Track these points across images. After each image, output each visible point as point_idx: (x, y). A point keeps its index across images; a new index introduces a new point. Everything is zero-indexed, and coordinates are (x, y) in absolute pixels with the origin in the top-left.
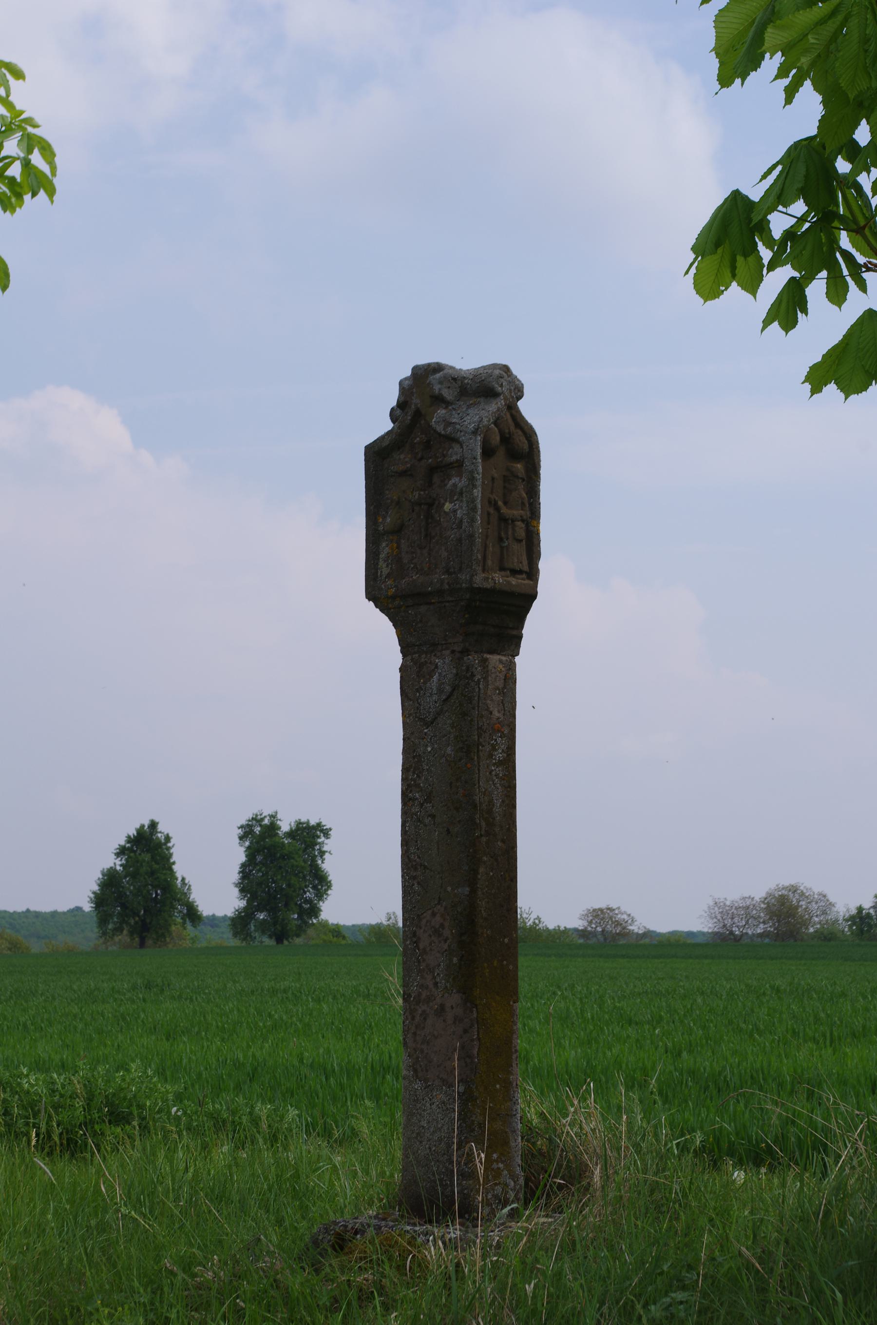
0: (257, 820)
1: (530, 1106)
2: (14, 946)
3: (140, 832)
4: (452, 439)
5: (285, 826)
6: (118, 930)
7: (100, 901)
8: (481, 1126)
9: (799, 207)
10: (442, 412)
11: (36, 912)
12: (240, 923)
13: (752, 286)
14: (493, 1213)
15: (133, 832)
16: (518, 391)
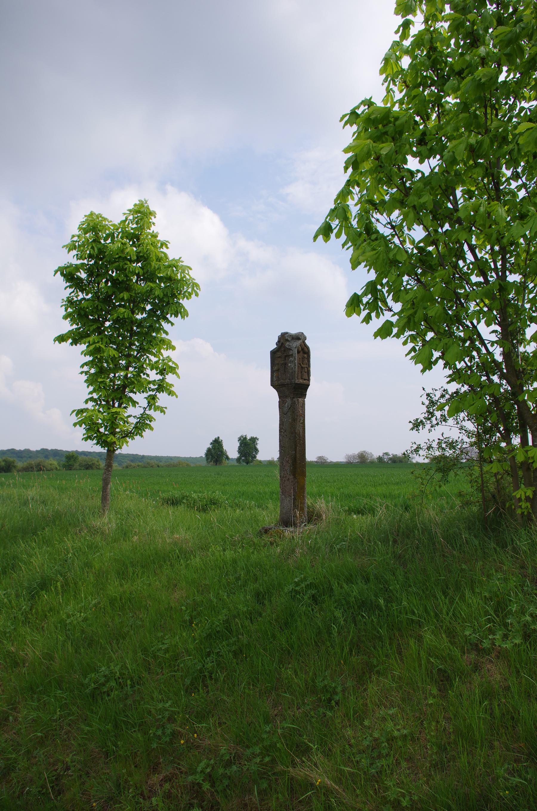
0: (242, 436)
1: (309, 501)
2: (187, 465)
3: (216, 439)
4: (290, 349)
5: (248, 438)
6: (211, 461)
7: (207, 455)
8: (298, 505)
9: (369, 296)
10: (288, 343)
11: (52, 450)
12: (238, 460)
13: (359, 314)
14: (301, 525)
15: (214, 439)
16: (305, 338)
